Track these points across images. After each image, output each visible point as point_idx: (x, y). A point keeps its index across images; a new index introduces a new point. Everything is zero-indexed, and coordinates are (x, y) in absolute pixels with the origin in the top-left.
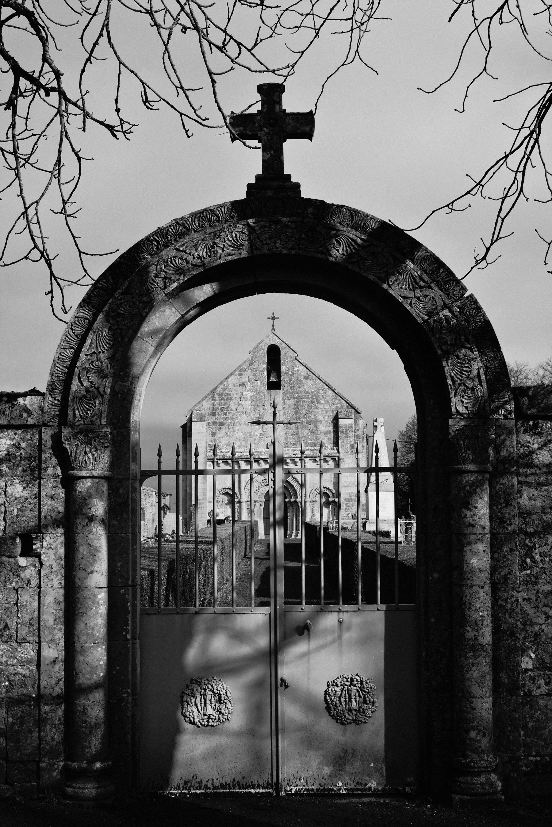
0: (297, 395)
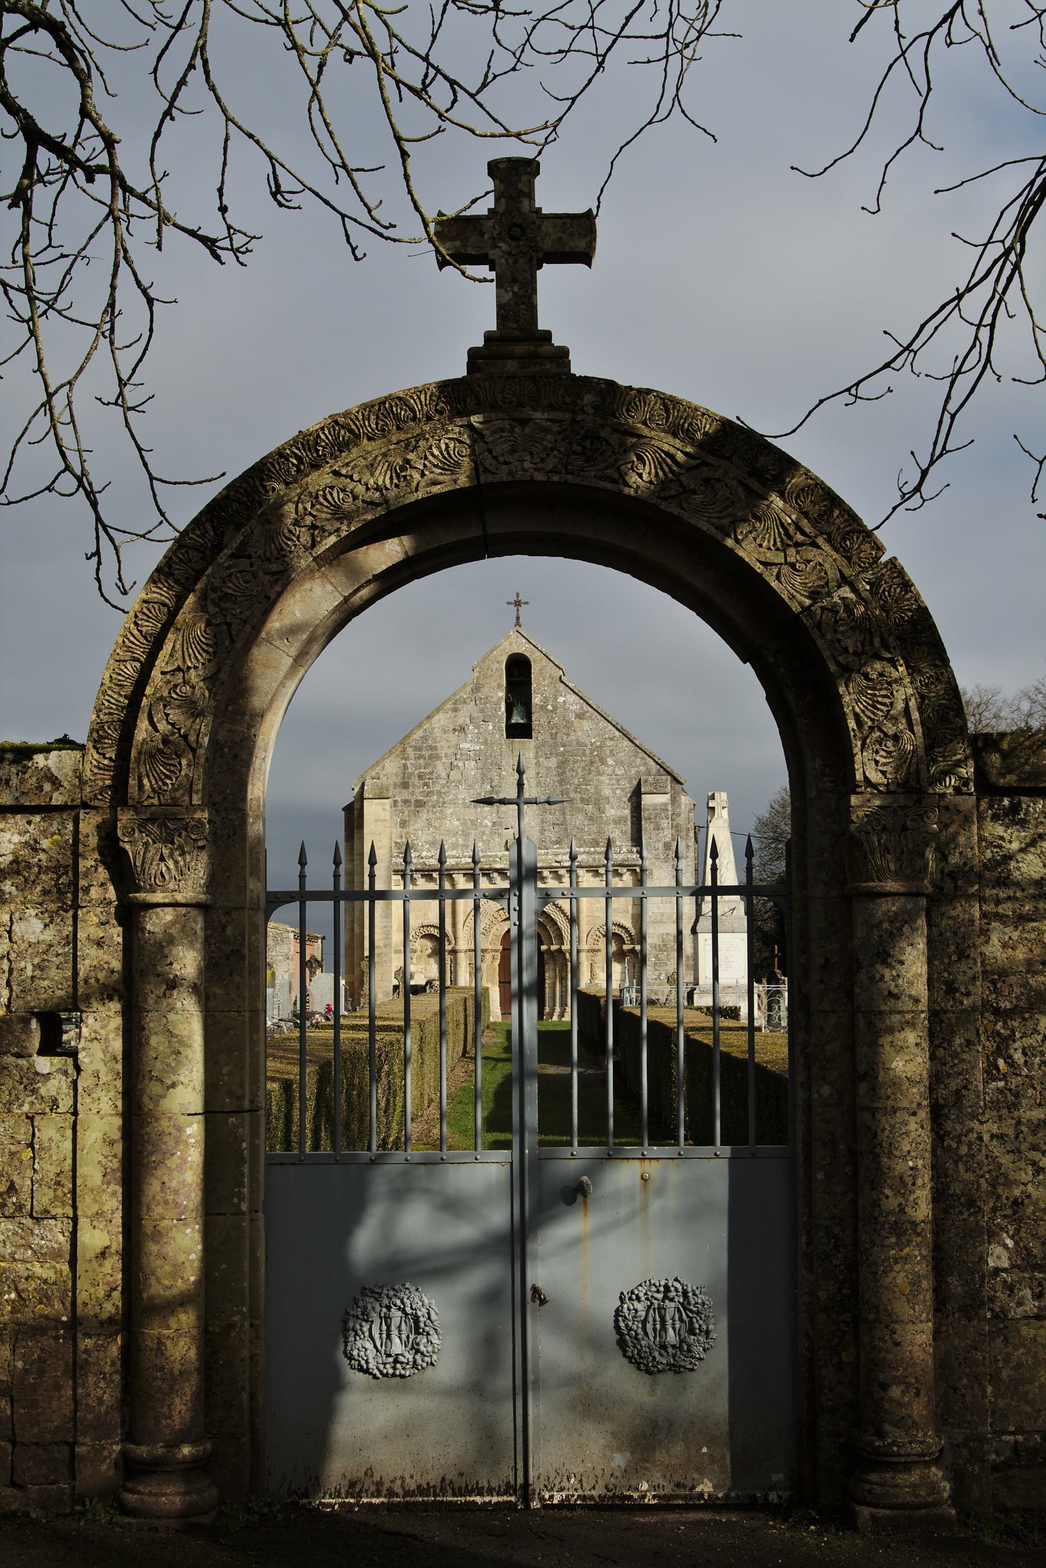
0: (562, 749)
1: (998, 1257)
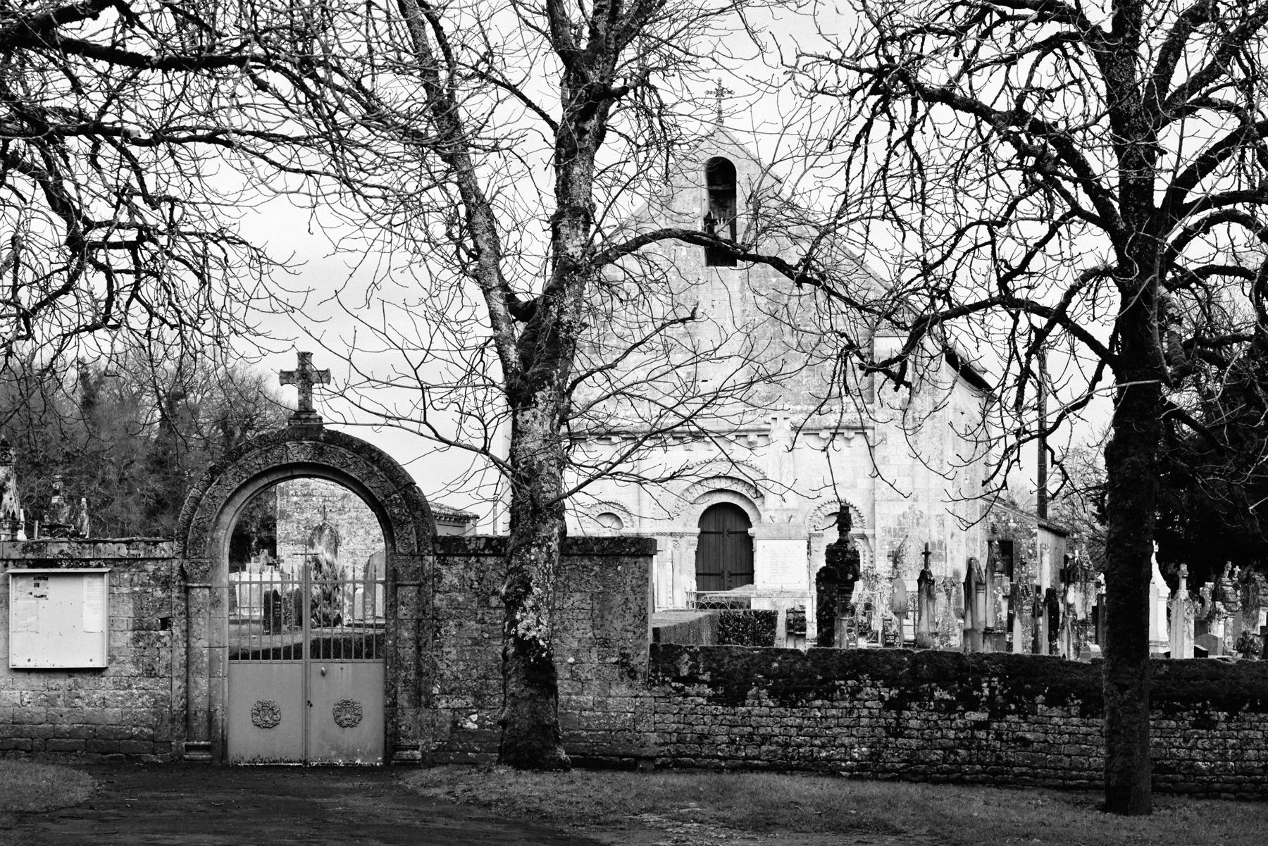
1: (436, 691)
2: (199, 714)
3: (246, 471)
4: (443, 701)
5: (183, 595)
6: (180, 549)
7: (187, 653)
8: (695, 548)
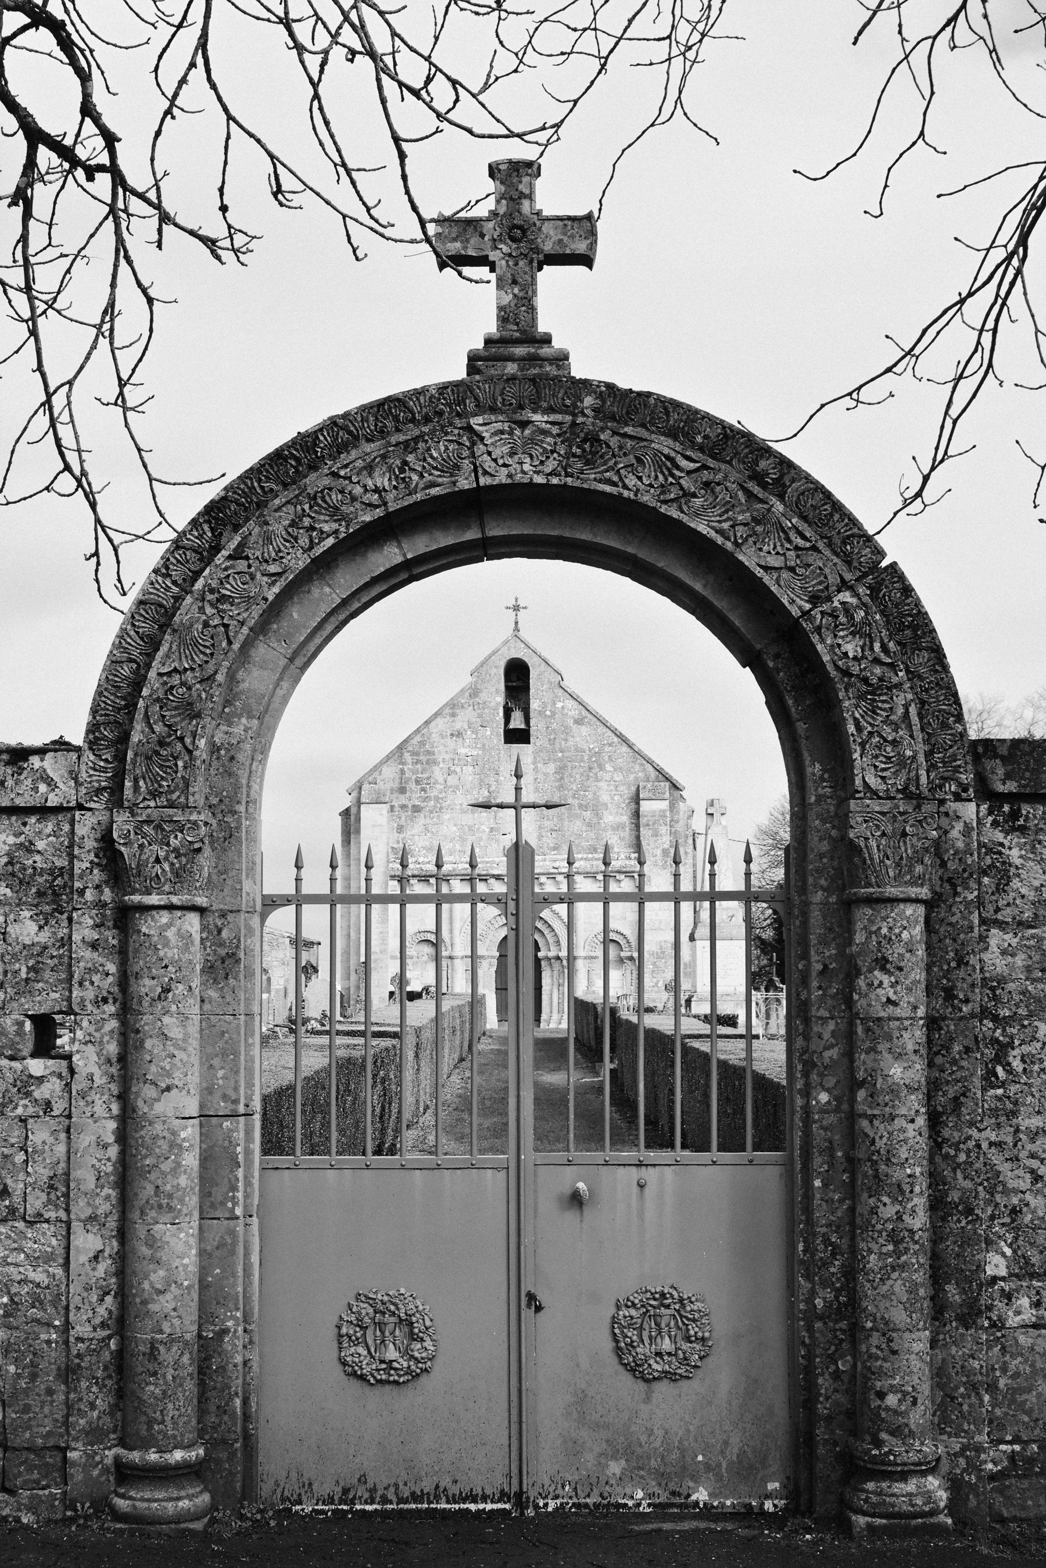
1: (996, 1265)
2: (168, 1356)
3: (335, 513)
4: (1024, 1302)
5: (111, 938)
6: (103, 780)
7: (122, 1137)
8: (495, 968)
